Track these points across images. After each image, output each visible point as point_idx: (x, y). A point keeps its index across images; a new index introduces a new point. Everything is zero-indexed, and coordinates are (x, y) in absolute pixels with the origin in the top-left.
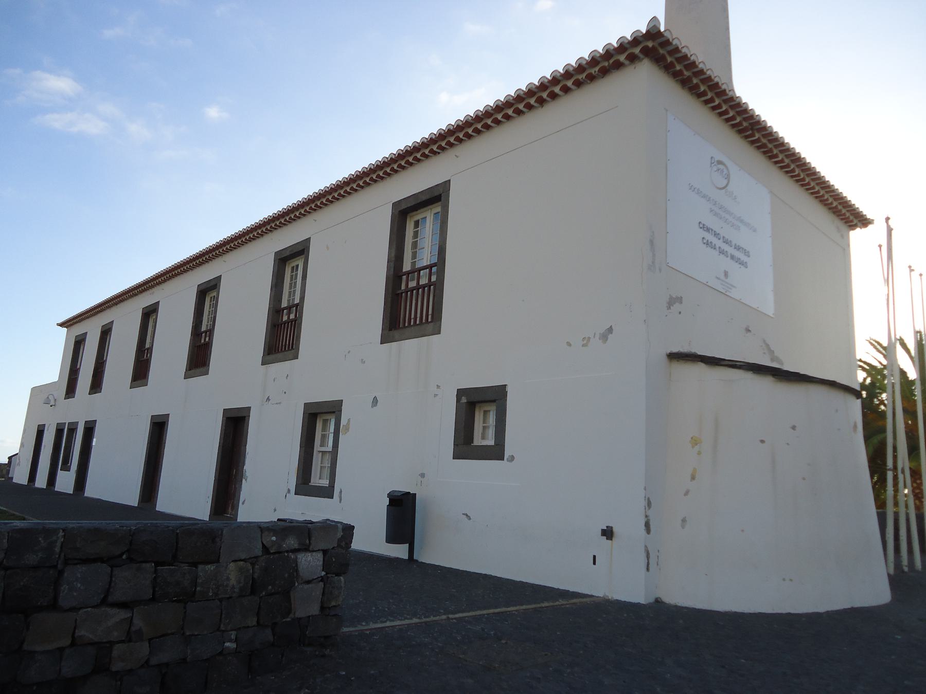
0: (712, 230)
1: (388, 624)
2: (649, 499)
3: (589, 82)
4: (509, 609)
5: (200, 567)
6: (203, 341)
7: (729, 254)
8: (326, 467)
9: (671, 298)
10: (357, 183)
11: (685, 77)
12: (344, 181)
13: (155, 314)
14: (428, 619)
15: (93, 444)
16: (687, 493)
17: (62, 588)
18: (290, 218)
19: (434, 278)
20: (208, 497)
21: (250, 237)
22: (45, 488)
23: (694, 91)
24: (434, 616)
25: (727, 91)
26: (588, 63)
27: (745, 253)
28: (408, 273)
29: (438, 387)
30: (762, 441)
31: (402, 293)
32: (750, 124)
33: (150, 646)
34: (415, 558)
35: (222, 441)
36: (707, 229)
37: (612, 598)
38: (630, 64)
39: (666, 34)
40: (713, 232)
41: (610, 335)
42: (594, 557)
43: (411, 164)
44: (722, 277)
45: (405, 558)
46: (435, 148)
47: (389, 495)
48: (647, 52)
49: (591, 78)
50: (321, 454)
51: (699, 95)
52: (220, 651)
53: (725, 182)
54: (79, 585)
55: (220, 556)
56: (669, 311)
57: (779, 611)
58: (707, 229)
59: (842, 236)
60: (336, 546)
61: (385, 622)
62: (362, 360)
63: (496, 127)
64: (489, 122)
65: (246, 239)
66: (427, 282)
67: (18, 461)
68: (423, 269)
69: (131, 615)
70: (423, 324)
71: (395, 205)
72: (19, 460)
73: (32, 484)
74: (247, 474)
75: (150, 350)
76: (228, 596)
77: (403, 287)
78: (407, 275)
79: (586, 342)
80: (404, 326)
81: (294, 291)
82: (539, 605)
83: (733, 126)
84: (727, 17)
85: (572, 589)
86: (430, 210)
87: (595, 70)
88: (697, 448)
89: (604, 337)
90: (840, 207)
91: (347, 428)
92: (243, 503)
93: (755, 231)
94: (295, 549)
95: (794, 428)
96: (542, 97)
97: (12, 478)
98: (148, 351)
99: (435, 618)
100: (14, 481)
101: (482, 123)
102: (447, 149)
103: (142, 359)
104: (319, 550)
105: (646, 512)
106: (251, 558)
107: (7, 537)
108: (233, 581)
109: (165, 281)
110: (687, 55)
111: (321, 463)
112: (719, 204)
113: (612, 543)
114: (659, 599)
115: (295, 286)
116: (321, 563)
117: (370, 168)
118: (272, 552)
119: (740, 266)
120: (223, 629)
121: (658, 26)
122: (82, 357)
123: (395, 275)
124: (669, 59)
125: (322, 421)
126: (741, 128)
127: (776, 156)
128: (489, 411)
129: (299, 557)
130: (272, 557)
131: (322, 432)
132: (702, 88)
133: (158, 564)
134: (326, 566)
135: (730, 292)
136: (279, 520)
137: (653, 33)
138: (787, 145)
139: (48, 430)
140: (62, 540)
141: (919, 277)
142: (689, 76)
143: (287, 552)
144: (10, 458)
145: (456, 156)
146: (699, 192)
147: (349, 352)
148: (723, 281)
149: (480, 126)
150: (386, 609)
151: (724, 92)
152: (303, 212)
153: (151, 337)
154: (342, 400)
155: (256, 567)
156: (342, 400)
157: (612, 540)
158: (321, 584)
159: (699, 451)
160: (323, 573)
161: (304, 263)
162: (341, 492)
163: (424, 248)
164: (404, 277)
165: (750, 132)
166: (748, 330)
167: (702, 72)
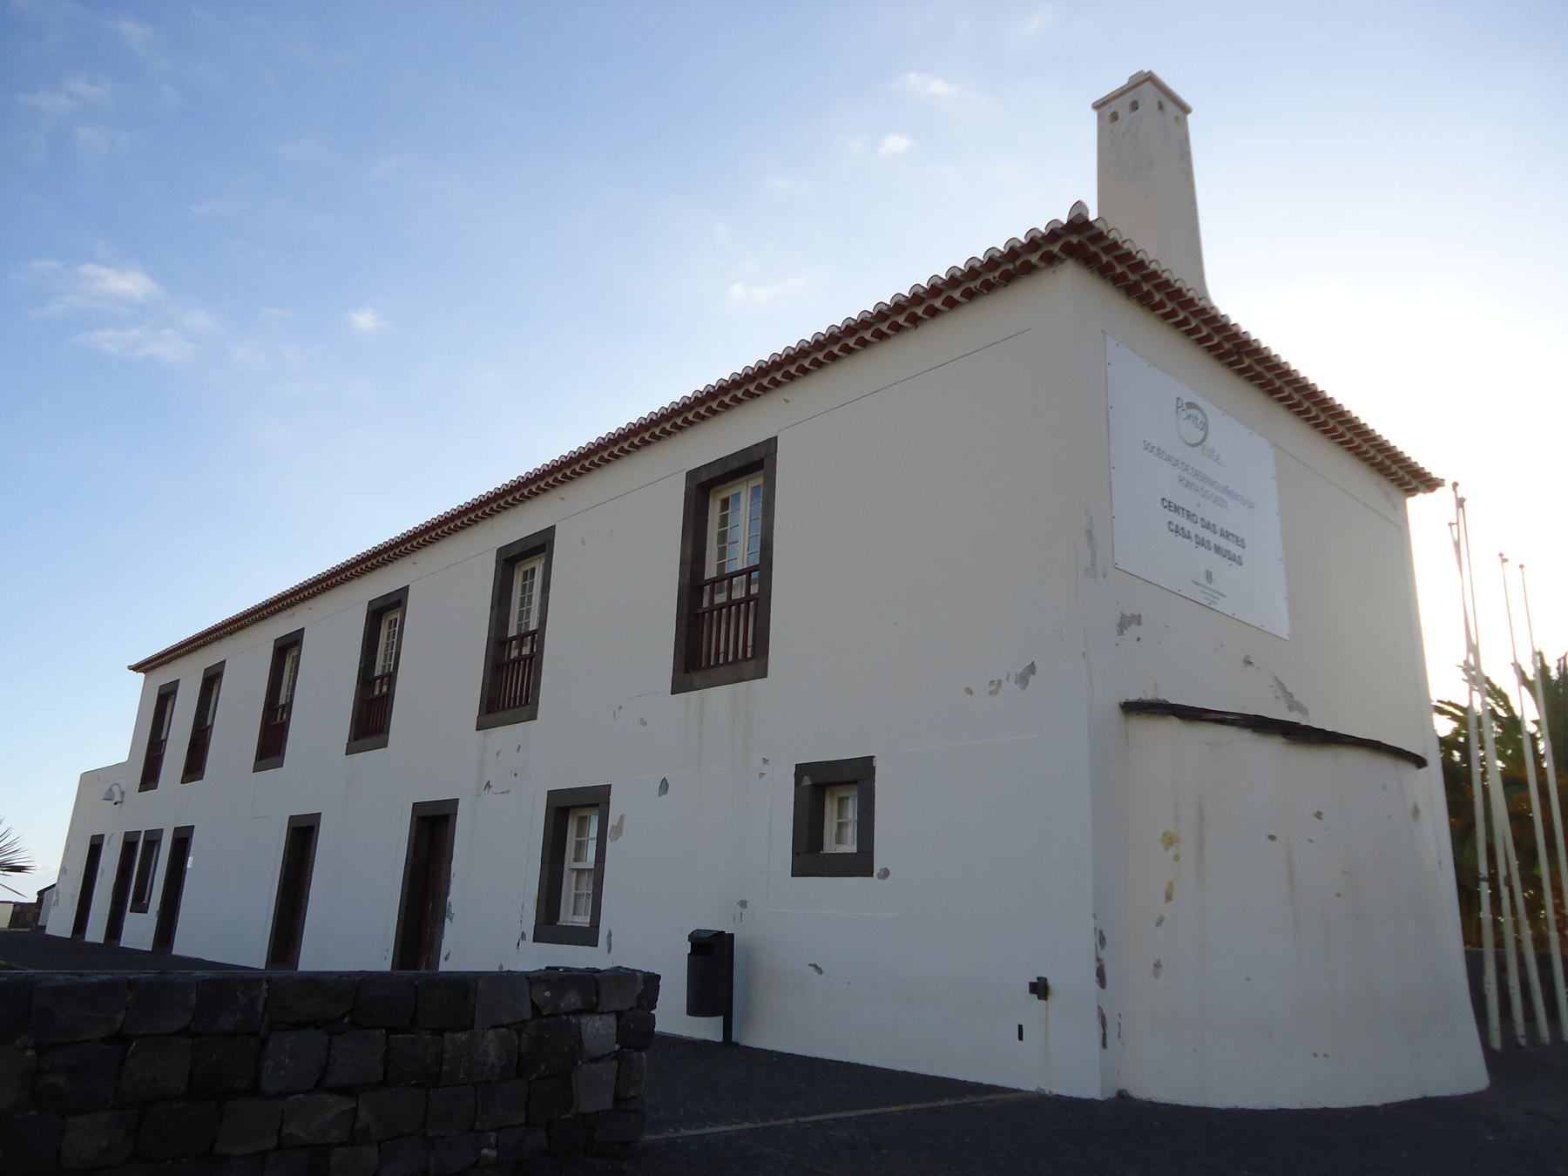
0: (1183, 509)
1: (707, 1130)
2: (1101, 932)
3: (985, 292)
4: (889, 1110)
5: (448, 1035)
6: (377, 693)
7: (1212, 545)
8: (583, 895)
9: (1123, 617)
10: (797, 364)
11: (1131, 283)
12: (609, 439)
13: (173, 696)
14: (766, 1124)
15: (188, 866)
16: (1159, 923)
17: (265, 1065)
19: (754, 589)
20: (387, 951)
22: (102, 942)
23: (1145, 301)
24: (775, 1120)
25: (1196, 300)
26: (983, 265)
27: (1237, 541)
28: (713, 582)
29: (765, 761)
30: (1272, 838)
31: (704, 613)
32: (1235, 345)
33: (379, 1153)
34: (734, 1039)
36: (1175, 507)
37: (1050, 1092)
38: (1047, 267)
39: (1097, 225)
40: (1185, 512)
41: (1032, 676)
42: (1020, 1027)
43: (715, 413)
44: (1203, 580)
45: (717, 1041)
46: (752, 388)
47: (692, 937)
48: (1072, 252)
49: (989, 287)
51: (1154, 307)
52: (474, 1161)
53: (1202, 434)
54: (287, 1061)
55: (474, 1018)
56: (1122, 637)
57: (1311, 1106)
58: (1175, 507)
59: (1395, 507)
60: (634, 1005)
61: (703, 1127)
62: (642, 720)
63: (846, 357)
64: (836, 349)
65: (449, 528)
66: (744, 596)
67: (54, 898)
69: (355, 1105)
72: (58, 895)
76: (484, 1079)
77: (706, 604)
79: (996, 687)
80: (709, 666)
81: (529, 611)
82: (936, 1104)
83: (1210, 349)
84: (1192, 186)
85: (986, 1081)
87: (993, 276)
88: (1172, 851)
89: (1023, 679)
90: (1388, 462)
91: (619, 830)
92: (446, 959)
93: (1251, 506)
94: (577, 1010)
95: (1319, 815)
97: (44, 928)
98: (283, 710)
99: (777, 1123)
100: (48, 931)
102: (771, 389)
103: (275, 723)
104: (611, 1012)
105: (1097, 952)
106: (515, 1023)
107: (195, 991)
108: (492, 1058)
109: (313, 595)
110: (1131, 252)
111: (577, 889)
112: (1192, 468)
113: (1047, 1007)
114: (1124, 1093)
115: (530, 603)
116: (614, 1031)
117: (651, 419)
118: (545, 1014)
119: (1230, 562)
120: (479, 1128)
121: (1084, 213)
123: (693, 585)
124: (1105, 259)
125: (576, 818)
126: (1220, 351)
127: (1280, 390)
128: (847, 798)
129: (582, 1021)
130: (545, 1021)
131: (577, 837)
132: (1157, 297)
133: (391, 1031)
134: (621, 1036)
135: (1217, 604)
136: (547, 968)
137: (1078, 223)
138: (1295, 374)
139: (108, 845)
140: (266, 995)
141: (1520, 569)
142: (1136, 281)
143: (567, 1014)
144: (41, 893)
145: (785, 400)
146: (1160, 453)
147: (620, 708)
148: (1205, 587)
149: (869, 335)
150: (702, 1112)
151: (1191, 301)
152: (542, 486)
153: (288, 686)
154: (610, 785)
155: (524, 1036)
156: (610, 785)
157: (1046, 999)
158: (615, 1063)
159: (1176, 856)
160: (617, 1047)
161: (545, 565)
162: (1439, 701)
163: (736, 542)
164: (708, 588)
165: (1235, 357)
166: (1248, 662)
167: (1155, 274)
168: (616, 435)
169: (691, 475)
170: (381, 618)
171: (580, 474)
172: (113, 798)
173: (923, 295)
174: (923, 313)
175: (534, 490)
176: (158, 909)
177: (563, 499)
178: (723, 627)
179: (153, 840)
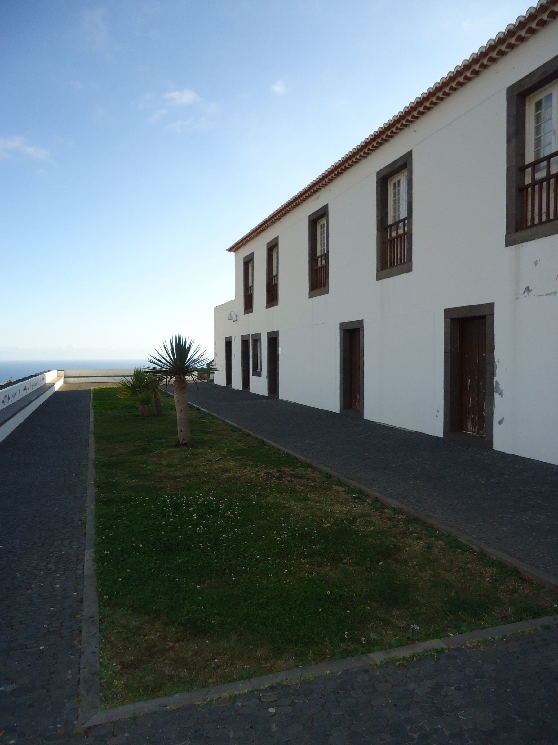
18: (338, 172)
21: (345, 166)
28: (391, 226)
35: (449, 347)
43: (442, 99)
74: (502, 387)
80: (533, 225)
92: (500, 422)
97: (213, 380)
109: (331, 181)
122: (253, 276)
139: (234, 341)
164: (320, 259)
168: (421, 99)
169: (510, 90)
170: (316, 223)
171: (396, 133)
172: (233, 319)
173: (546, 5)
174: (395, 130)
175: (347, 166)
177: (415, 131)
179: (257, 339)
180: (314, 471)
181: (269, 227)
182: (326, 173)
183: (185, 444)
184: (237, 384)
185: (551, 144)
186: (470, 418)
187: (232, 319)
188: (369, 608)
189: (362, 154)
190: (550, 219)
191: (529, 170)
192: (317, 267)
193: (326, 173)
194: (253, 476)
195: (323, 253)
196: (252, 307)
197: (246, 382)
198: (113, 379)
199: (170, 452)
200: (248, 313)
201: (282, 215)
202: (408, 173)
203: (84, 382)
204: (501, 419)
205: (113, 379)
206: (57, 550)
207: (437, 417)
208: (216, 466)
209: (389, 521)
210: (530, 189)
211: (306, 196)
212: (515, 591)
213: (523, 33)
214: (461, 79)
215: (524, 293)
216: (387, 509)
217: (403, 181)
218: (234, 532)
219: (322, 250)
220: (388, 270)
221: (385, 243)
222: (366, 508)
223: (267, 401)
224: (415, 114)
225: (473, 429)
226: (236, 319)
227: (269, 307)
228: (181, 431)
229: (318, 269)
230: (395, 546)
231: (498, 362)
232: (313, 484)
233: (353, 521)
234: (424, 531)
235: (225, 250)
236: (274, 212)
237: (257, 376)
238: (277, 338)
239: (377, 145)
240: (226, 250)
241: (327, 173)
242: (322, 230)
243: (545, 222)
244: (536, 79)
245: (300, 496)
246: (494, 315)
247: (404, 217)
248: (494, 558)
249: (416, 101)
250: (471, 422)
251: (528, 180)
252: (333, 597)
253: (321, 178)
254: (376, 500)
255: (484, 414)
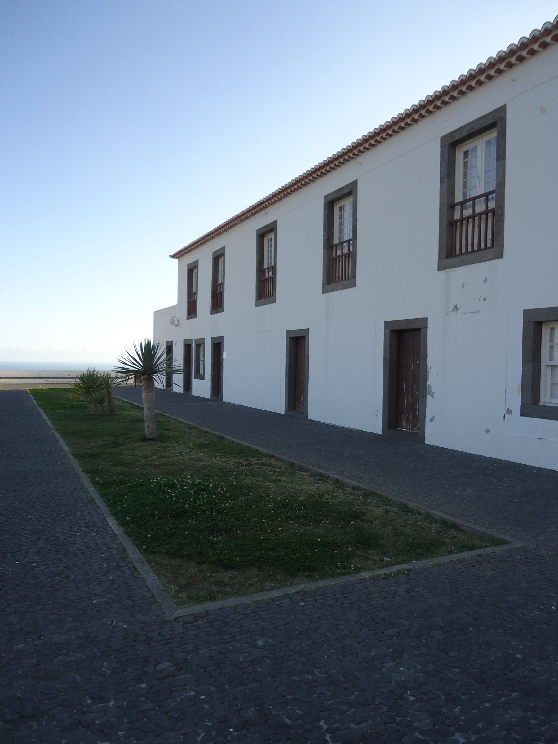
18: (288, 193)
28: (336, 245)
35: (388, 355)
43: (373, 146)
50: (550, 368)
63: (415, 124)
68: (477, 199)
70: (464, 254)
71: (325, 197)
73: (169, 389)
74: (433, 389)
75: (222, 284)
78: (486, 196)
86: (347, 200)
92: (432, 420)
96: (445, 100)
101: (476, 80)
139: (176, 345)
149: (316, 175)
164: (267, 270)
172: (175, 323)
176: (210, 378)
177: (361, 164)
178: (476, 230)
179: (200, 344)
180: (277, 461)
181: (215, 237)
182: (276, 193)
183: (152, 439)
184: (178, 386)
185: (476, 187)
186: (405, 417)
187: (174, 324)
188: (351, 549)
189: (311, 178)
190: (475, 250)
191: (458, 208)
192: (264, 278)
193: (276, 193)
194: (225, 464)
195: (270, 266)
196: (195, 313)
197: (188, 385)
198: (47, 381)
199: (140, 445)
200: (191, 318)
201: (230, 227)
202: (353, 199)
203: (16, 383)
204: (432, 418)
205: (47, 381)
206: (82, 519)
207: (376, 416)
208: (188, 457)
209: (351, 495)
210: (458, 223)
211: (255, 211)
212: (455, 538)
213: (455, 94)
214: (402, 125)
215: (453, 310)
216: (347, 487)
217: (348, 204)
218: (229, 503)
219: (269, 262)
220: (334, 285)
221: (331, 260)
222: (329, 486)
223: (212, 403)
224: (361, 149)
225: (407, 427)
226: (178, 324)
227: (214, 314)
228: (149, 427)
229: (265, 280)
230: (361, 512)
231: (430, 368)
232: (279, 470)
233: (322, 495)
234: (380, 501)
235: (168, 256)
236: (222, 224)
237: (200, 379)
238: (222, 343)
239: (326, 172)
240: (170, 256)
241: (277, 193)
242: (270, 244)
243: (470, 252)
244: (465, 133)
245: (272, 479)
246: (427, 328)
247: (348, 239)
248: (437, 517)
249: (363, 138)
250: (406, 420)
251: (457, 216)
252: (323, 543)
253: (270, 196)
254: (337, 481)
255: (417, 413)
